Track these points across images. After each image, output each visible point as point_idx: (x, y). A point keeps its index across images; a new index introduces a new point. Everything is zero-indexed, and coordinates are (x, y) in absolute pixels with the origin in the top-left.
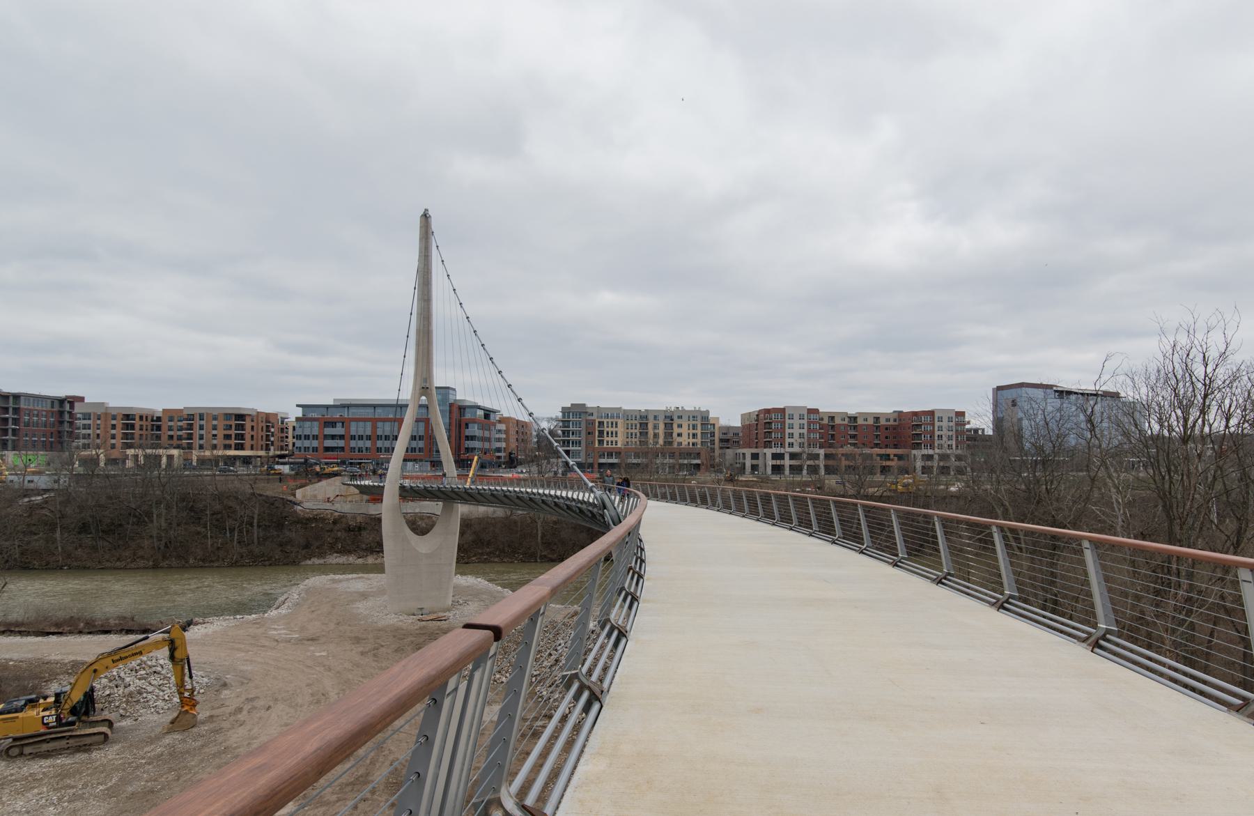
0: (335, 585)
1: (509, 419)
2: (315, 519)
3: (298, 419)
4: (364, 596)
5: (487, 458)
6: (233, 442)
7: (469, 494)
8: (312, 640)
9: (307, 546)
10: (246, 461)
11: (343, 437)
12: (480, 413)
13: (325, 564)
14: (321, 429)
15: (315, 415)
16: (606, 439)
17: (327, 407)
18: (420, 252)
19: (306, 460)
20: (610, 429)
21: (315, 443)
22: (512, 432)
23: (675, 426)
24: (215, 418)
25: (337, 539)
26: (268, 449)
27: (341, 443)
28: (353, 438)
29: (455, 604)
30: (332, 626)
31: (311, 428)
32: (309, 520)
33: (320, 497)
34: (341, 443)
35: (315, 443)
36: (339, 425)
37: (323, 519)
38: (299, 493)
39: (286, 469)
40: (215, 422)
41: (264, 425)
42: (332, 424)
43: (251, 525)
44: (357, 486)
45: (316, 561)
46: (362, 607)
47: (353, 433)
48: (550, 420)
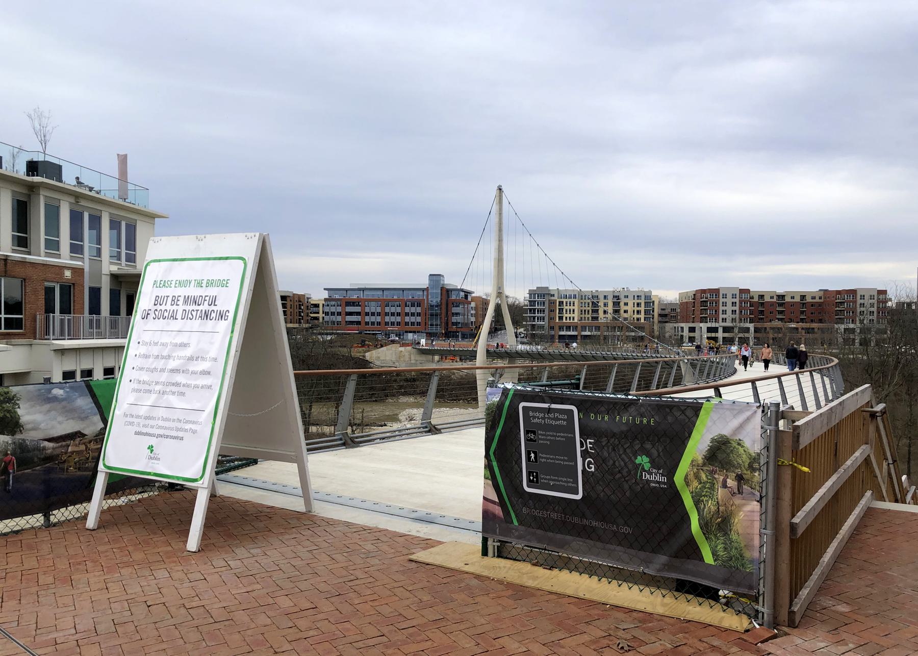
12: (462, 294)
15: (337, 297)
16: (565, 315)
17: (347, 290)
20: (568, 308)
23: (622, 304)
26: (300, 323)
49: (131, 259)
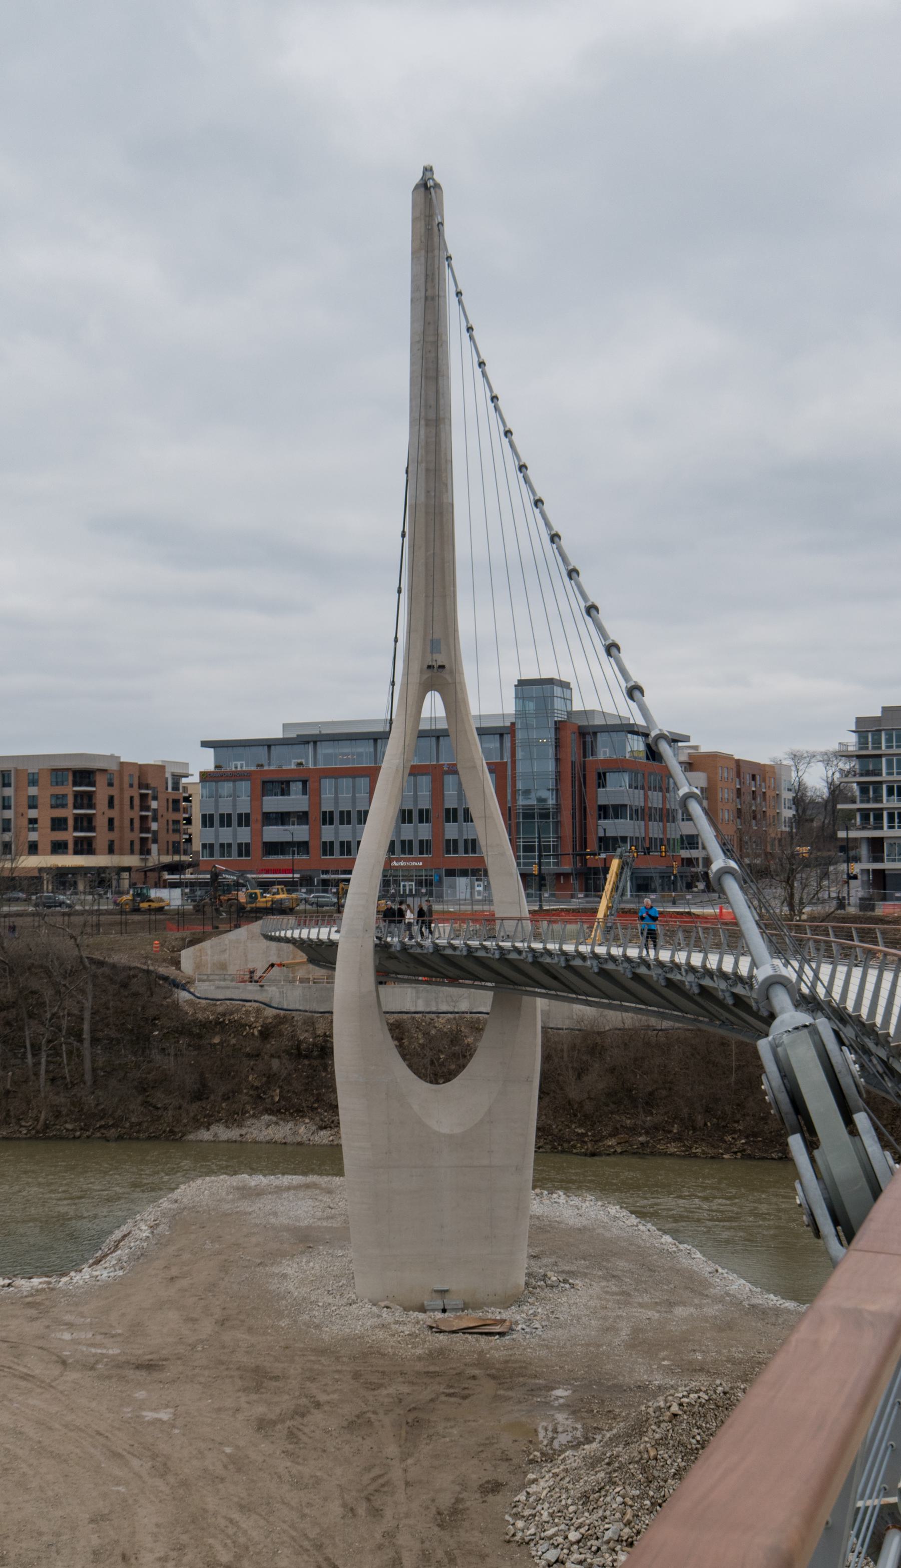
0: (244, 1206)
1: (714, 757)
2: (219, 1025)
3: (205, 777)
4: (306, 1240)
5: (652, 865)
6: (70, 835)
7: (547, 970)
8: (149, 1367)
9: (199, 1095)
10: (100, 879)
11: (281, 810)
12: (636, 745)
13: (240, 1143)
14: (255, 799)
15: (240, 765)
17: (269, 744)
18: (415, 289)
19: (215, 875)
21: (244, 835)
22: (726, 794)
24: (33, 781)
25: (271, 1078)
26: (145, 851)
27: (300, 832)
28: (327, 818)
29: (536, 1283)
30: (207, 1327)
31: (235, 796)
32: (206, 1026)
33: (232, 970)
34: (300, 832)
35: (244, 835)
36: (296, 787)
37: (239, 1026)
38: (187, 956)
39: (173, 898)
40: (33, 791)
41: (136, 793)
42: (282, 786)
43: (80, 1039)
44: (300, 944)
45: (223, 1133)
46: (294, 1275)
47: (326, 807)
48: (827, 759)
49: (376, 762)
